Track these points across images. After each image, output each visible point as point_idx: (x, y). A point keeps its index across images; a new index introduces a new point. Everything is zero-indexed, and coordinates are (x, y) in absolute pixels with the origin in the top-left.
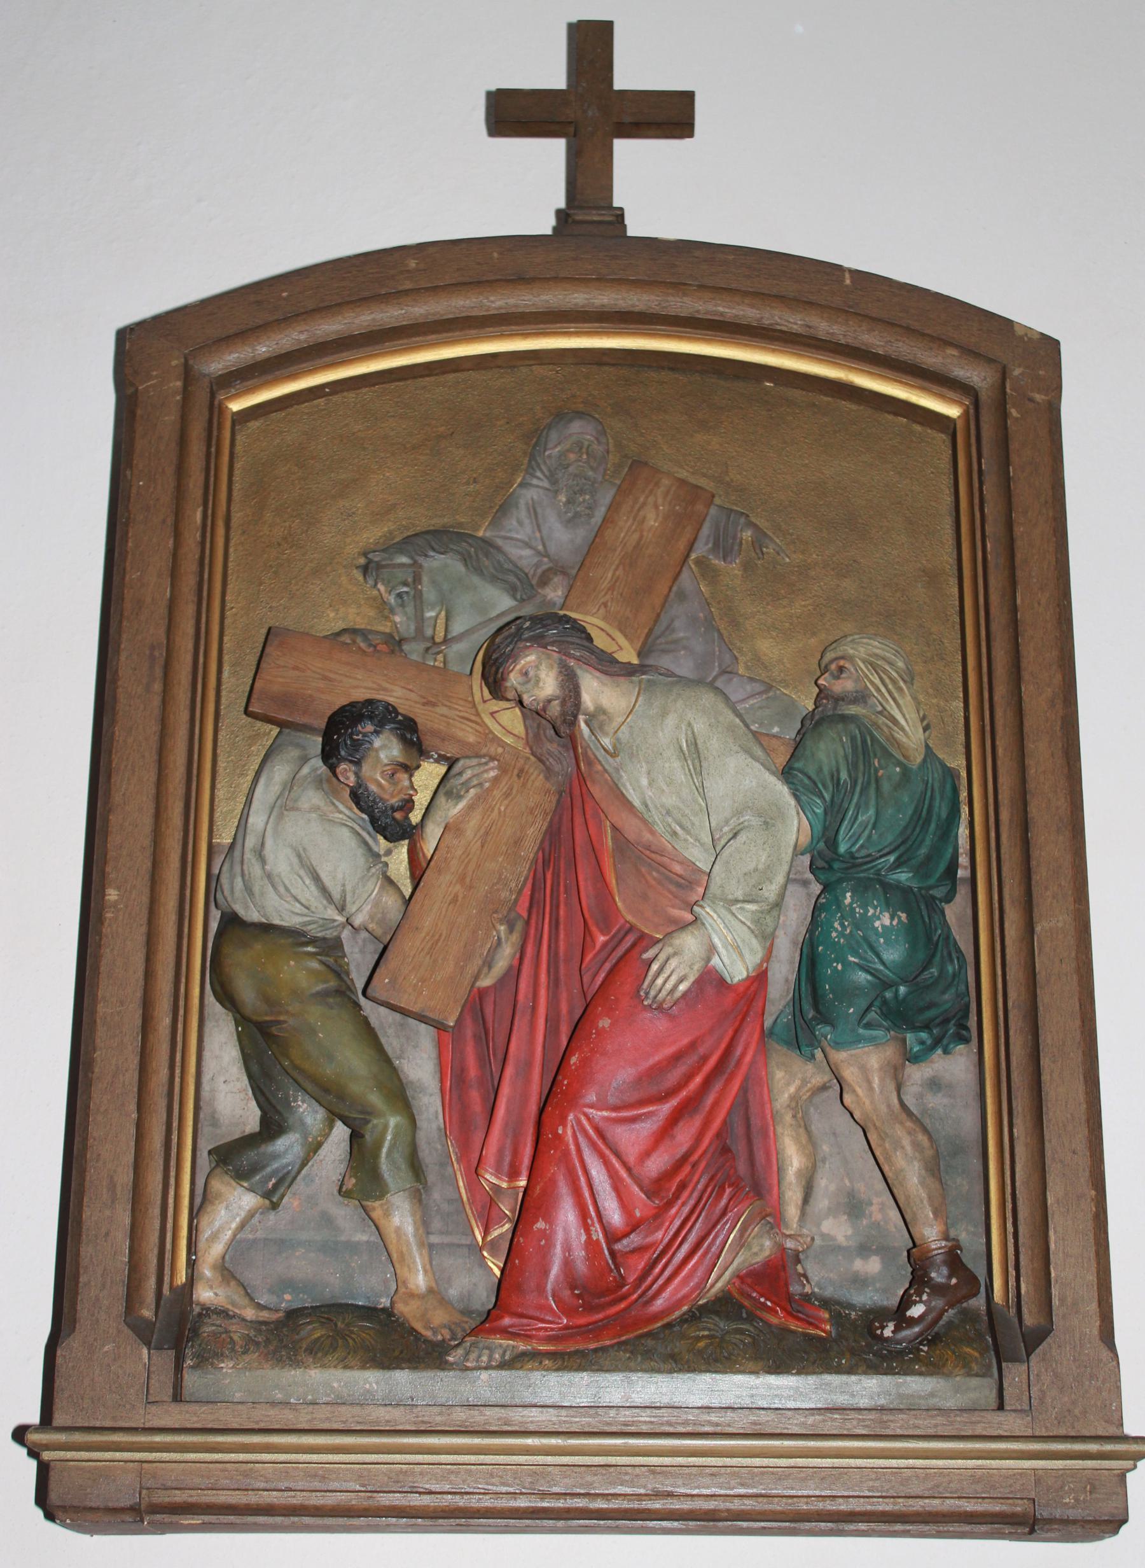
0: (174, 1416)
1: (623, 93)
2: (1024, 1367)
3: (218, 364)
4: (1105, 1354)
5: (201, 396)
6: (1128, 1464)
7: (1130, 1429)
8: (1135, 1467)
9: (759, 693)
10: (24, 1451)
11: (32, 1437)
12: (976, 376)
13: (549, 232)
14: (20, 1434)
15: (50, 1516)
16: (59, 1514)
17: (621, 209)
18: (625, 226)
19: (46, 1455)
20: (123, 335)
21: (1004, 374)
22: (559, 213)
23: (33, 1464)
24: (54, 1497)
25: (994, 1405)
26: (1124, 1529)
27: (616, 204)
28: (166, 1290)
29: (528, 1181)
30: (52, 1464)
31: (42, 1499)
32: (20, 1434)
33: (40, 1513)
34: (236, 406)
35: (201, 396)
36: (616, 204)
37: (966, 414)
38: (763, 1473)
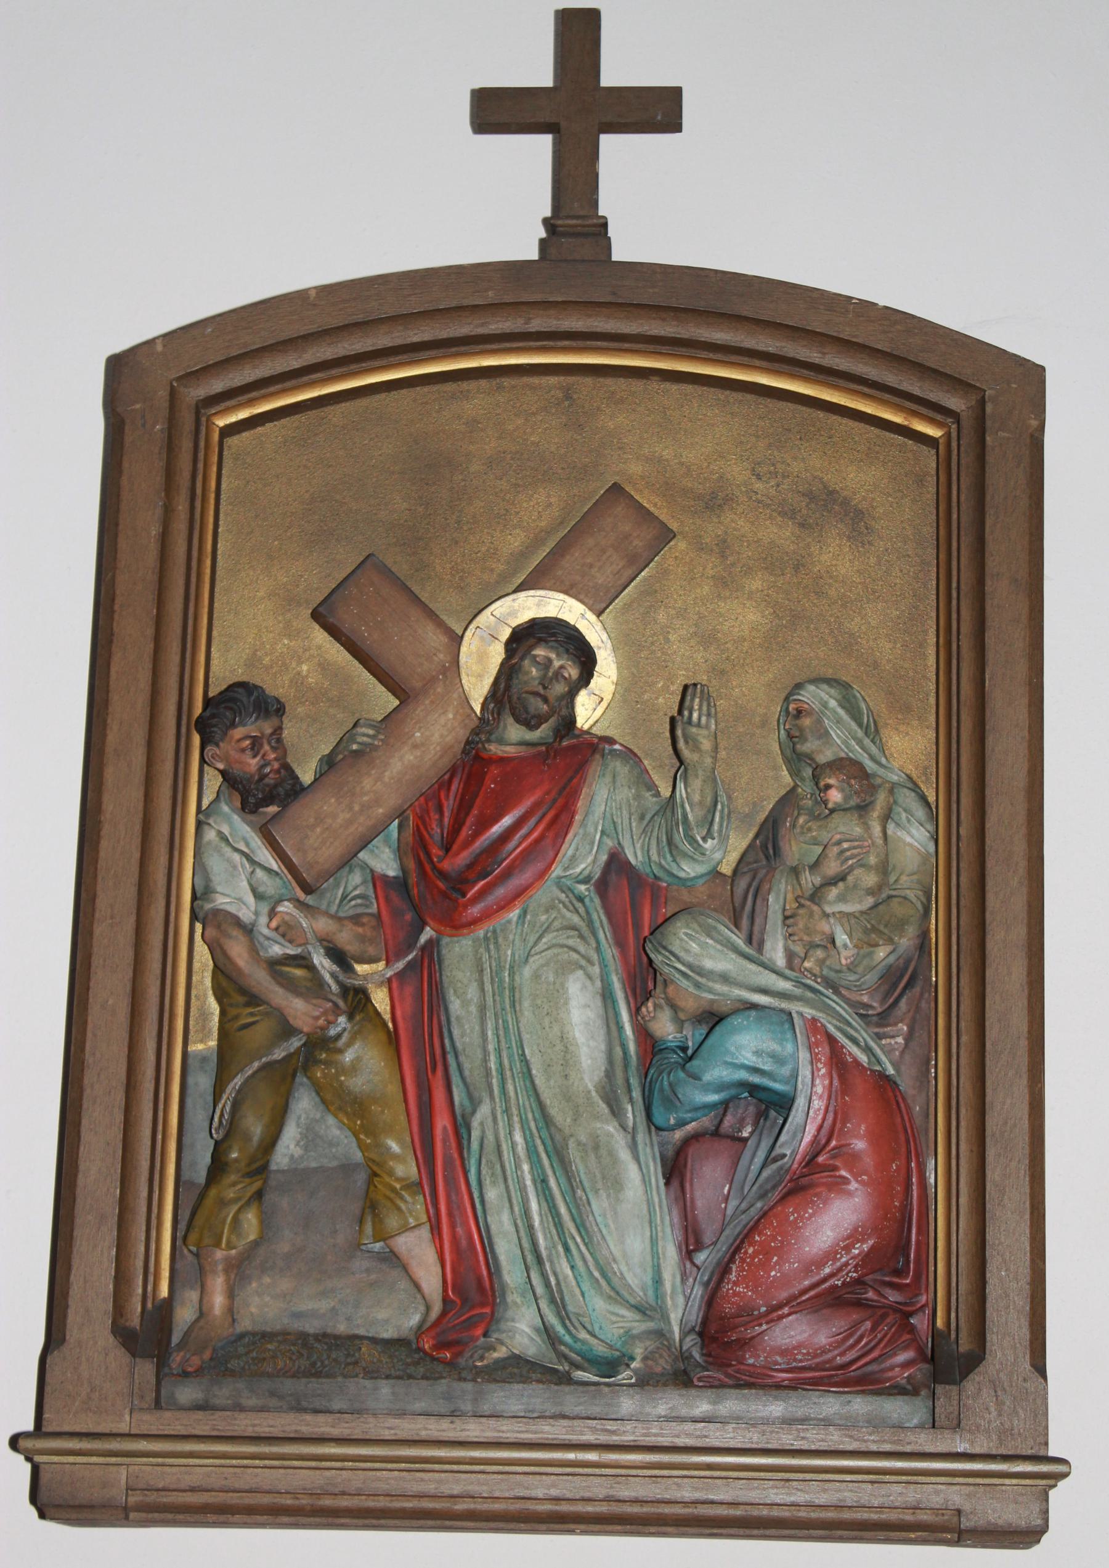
0: (151, 1422)
1: (611, 90)
2: (954, 1388)
3: (201, 391)
4: (1041, 1380)
5: (187, 420)
6: (1051, 1482)
7: (1052, 1453)
8: (1055, 1486)
9: (681, 1347)
10: (21, 1458)
11: (23, 1443)
12: (955, 402)
13: (532, 254)
14: (15, 1442)
15: (42, 1515)
16: (47, 1511)
17: (604, 218)
18: (610, 238)
19: (38, 1459)
20: (117, 366)
21: (982, 403)
22: (546, 222)
23: (28, 1467)
24: (43, 1496)
25: (931, 1425)
26: (1045, 1538)
27: (601, 213)
28: (149, 1305)
29: (355, 855)
30: (42, 1466)
31: (34, 1499)
32: (15, 1442)
33: (33, 1512)
34: (221, 422)
35: (187, 420)
36: (601, 213)
37: (948, 435)
38: (929, 1032)
